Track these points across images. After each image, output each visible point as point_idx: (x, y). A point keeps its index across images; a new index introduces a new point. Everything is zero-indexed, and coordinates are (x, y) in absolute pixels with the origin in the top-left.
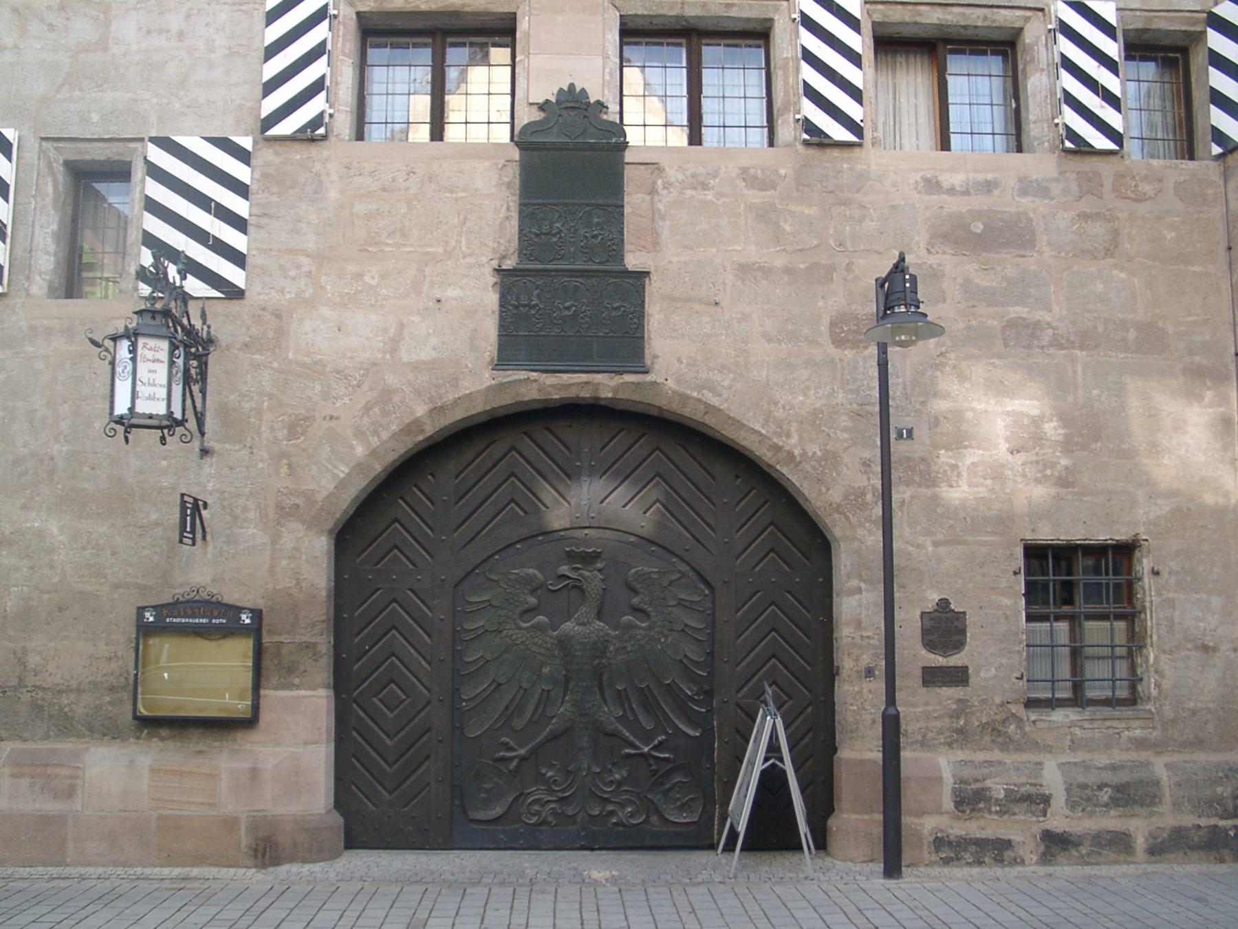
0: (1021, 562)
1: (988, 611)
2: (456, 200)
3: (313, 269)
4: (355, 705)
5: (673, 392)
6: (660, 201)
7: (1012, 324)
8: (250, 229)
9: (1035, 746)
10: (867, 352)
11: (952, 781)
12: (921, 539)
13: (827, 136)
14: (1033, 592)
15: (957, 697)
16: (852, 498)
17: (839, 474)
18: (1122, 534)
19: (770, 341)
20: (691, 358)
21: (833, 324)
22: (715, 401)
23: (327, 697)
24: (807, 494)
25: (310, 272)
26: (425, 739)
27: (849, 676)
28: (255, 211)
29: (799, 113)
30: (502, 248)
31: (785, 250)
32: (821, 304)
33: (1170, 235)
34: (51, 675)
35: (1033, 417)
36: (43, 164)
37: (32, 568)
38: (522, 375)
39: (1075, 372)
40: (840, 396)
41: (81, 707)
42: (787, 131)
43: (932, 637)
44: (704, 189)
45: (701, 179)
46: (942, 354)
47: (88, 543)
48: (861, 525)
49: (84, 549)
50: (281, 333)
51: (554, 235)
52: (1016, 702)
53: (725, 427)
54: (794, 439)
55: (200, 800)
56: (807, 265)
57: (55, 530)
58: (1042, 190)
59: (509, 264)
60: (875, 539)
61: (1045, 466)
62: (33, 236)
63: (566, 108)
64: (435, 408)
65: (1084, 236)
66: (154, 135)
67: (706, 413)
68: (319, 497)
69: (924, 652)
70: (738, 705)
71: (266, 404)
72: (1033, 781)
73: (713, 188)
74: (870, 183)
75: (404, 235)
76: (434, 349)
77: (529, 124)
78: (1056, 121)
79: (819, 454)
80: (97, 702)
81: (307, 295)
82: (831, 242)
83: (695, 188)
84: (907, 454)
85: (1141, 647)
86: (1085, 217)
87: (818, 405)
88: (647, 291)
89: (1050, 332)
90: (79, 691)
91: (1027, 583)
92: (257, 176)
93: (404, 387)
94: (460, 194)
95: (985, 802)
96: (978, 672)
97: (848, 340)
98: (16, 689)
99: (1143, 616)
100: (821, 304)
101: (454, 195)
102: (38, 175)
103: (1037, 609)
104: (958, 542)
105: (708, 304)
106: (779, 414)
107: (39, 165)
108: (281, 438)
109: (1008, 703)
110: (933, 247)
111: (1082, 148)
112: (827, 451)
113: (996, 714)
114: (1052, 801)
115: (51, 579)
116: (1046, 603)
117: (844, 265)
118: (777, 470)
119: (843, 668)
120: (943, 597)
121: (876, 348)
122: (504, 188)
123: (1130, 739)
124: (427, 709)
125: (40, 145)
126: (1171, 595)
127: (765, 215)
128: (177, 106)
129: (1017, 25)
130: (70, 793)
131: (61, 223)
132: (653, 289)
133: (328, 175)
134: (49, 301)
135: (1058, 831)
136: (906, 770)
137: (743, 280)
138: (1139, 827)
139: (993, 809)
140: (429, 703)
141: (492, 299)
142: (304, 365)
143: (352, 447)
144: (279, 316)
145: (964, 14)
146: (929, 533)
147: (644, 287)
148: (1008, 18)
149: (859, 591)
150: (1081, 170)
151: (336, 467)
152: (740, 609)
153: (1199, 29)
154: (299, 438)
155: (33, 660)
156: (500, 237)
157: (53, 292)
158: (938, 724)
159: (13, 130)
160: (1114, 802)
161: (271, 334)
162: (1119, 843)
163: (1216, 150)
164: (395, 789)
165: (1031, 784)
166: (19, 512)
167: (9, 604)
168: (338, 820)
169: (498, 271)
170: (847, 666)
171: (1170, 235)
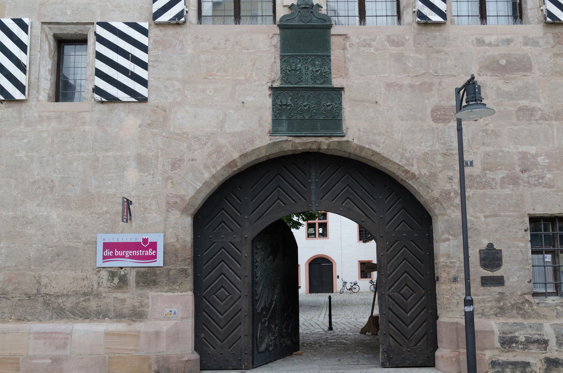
0: (527, 225)
1: (513, 249)
2: (250, 54)
3: (181, 87)
4: (204, 299)
5: (356, 145)
6: (348, 53)
7: (521, 109)
8: (149, 68)
9: (538, 315)
10: (450, 124)
11: (498, 333)
12: (478, 214)
13: (429, 19)
14: (534, 239)
15: (499, 291)
16: (444, 195)
17: (437, 183)
19: (402, 120)
20: (365, 129)
21: (433, 111)
23: (192, 295)
24: (421, 193)
25: (180, 89)
26: (239, 314)
27: (445, 281)
28: (151, 59)
29: (415, 8)
30: (273, 77)
31: (409, 76)
34: (53, 287)
35: (532, 154)
36: (43, 36)
37: (43, 235)
38: (285, 138)
39: (553, 132)
40: (437, 146)
41: (68, 304)
42: (408, 17)
43: (486, 262)
44: (369, 47)
45: (368, 42)
46: (486, 124)
47: (72, 222)
48: (449, 208)
49: (69, 225)
50: (166, 119)
51: (298, 71)
52: (528, 293)
53: (382, 161)
55: (130, 348)
56: (419, 83)
57: (55, 216)
58: (535, 43)
59: (276, 85)
60: (458, 214)
61: (539, 178)
62: (39, 71)
63: (302, 8)
64: (243, 155)
65: (556, 65)
66: (99, 21)
67: (372, 155)
68: (187, 198)
69: (481, 269)
71: (160, 153)
72: (539, 333)
74: (450, 42)
75: (225, 71)
76: (242, 126)
77: (284, 16)
78: (542, 8)
79: (427, 174)
80: (77, 301)
81: (179, 100)
83: (365, 47)
84: (471, 173)
87: (426, 151)
88: (343, 96)
89: (540, 112)
90: (68, 295)
91: (531, 235)
92: (151, 41)
93: (227, 145)
94: (252, 51)
95: (516, 344)
96: (509, 279)
97: (440, 119)
98: (35, 295)
101: (249, 51)
102: (41, 41)
104: (496, 216)
105: (373, 103)
106: (408, 155)
107: (41, 36)
108: (168, 170)
109: (524, 294)
110: (481, 72)
112: (431, 172)
113: (518, 299)
114: (549, 343)
115: (53, 240)
117: (438, 82)
118: (406, 182)
119: (441, 277)
120: (490, 242)
121: (456, 122)
122: (273, 47)
124: (239, 300)
125: (42, 26)
127: (399, 58)
128: (110, 7)
130: (64, 346)
131: (53, 64)
132: (346, 96)
133: (187, 41)
134: (49, 103)
135: (553, 358)
136: (477, 327)
137: (389, 91)
139: (520, 347)
140: (240, 297)
141: (269, 102)
142: (178, 134)
143: (203, 174)
144: (165, 111)
146: (482, 211)
147: (341, 96)
149: (448, 240)
150: (554, 32)
151: (195, 184)
152: (389, 249)
154: (176, 170)
155: (44, 281)
156: (272, 72)
157: (49, 99)
158: (489, 304)
159: (28, 19)
161: (161, 119)
164: (224, 340)
165: (538, 334)
166: (36, 208)
167: (32, 253)
168: (196, 356)
169: (271, 88)
170: (443, 276)
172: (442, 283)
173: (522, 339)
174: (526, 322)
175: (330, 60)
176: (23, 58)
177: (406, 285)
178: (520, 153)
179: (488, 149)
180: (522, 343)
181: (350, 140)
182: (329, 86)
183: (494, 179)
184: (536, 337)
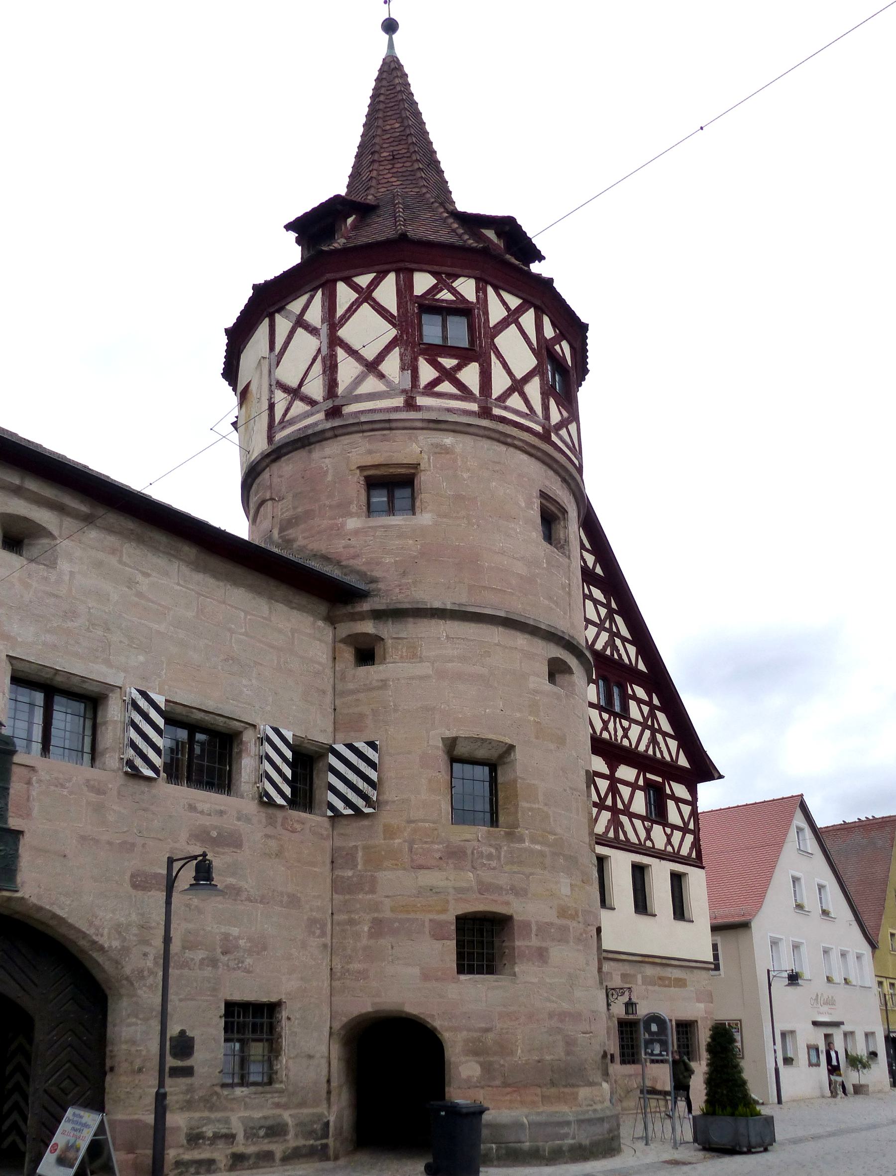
14: (228, 1028)
17: (130, 959)
18: (274, 999)
21: (132, 876)
45: (61, 781)
54: (105, 938)
58: (248, 820)
70: (45, 1091)
73: (67, 788)
78: (258, 785)
83: (56, 786)
85: (277, 1057)
86: (267, 836)
89: (246, 893)
99: (280, 1040)
103: (230, 1036)
104: (192, 1000)
116: (232, 1032)
123: (273, 1103)
126: (295, 1030)
127: (99, 809)
129: (240, 730)
138: (278, 1149)
149: (137, 1024)
160: (267, 1135)
162: (266, 1157)
163: (330, 813)
172: (121, 1074)
173: (210, 1134)
174: (213, 1116)
175: (8, 794)
176: (133, 734)
177: (69, 1077)
178: (222, 934)
179: (191, 926)
180: (209, 1139)
181: (27, 896)
182: (4, 826)
183: (193, 959)
184: (224, 1131)
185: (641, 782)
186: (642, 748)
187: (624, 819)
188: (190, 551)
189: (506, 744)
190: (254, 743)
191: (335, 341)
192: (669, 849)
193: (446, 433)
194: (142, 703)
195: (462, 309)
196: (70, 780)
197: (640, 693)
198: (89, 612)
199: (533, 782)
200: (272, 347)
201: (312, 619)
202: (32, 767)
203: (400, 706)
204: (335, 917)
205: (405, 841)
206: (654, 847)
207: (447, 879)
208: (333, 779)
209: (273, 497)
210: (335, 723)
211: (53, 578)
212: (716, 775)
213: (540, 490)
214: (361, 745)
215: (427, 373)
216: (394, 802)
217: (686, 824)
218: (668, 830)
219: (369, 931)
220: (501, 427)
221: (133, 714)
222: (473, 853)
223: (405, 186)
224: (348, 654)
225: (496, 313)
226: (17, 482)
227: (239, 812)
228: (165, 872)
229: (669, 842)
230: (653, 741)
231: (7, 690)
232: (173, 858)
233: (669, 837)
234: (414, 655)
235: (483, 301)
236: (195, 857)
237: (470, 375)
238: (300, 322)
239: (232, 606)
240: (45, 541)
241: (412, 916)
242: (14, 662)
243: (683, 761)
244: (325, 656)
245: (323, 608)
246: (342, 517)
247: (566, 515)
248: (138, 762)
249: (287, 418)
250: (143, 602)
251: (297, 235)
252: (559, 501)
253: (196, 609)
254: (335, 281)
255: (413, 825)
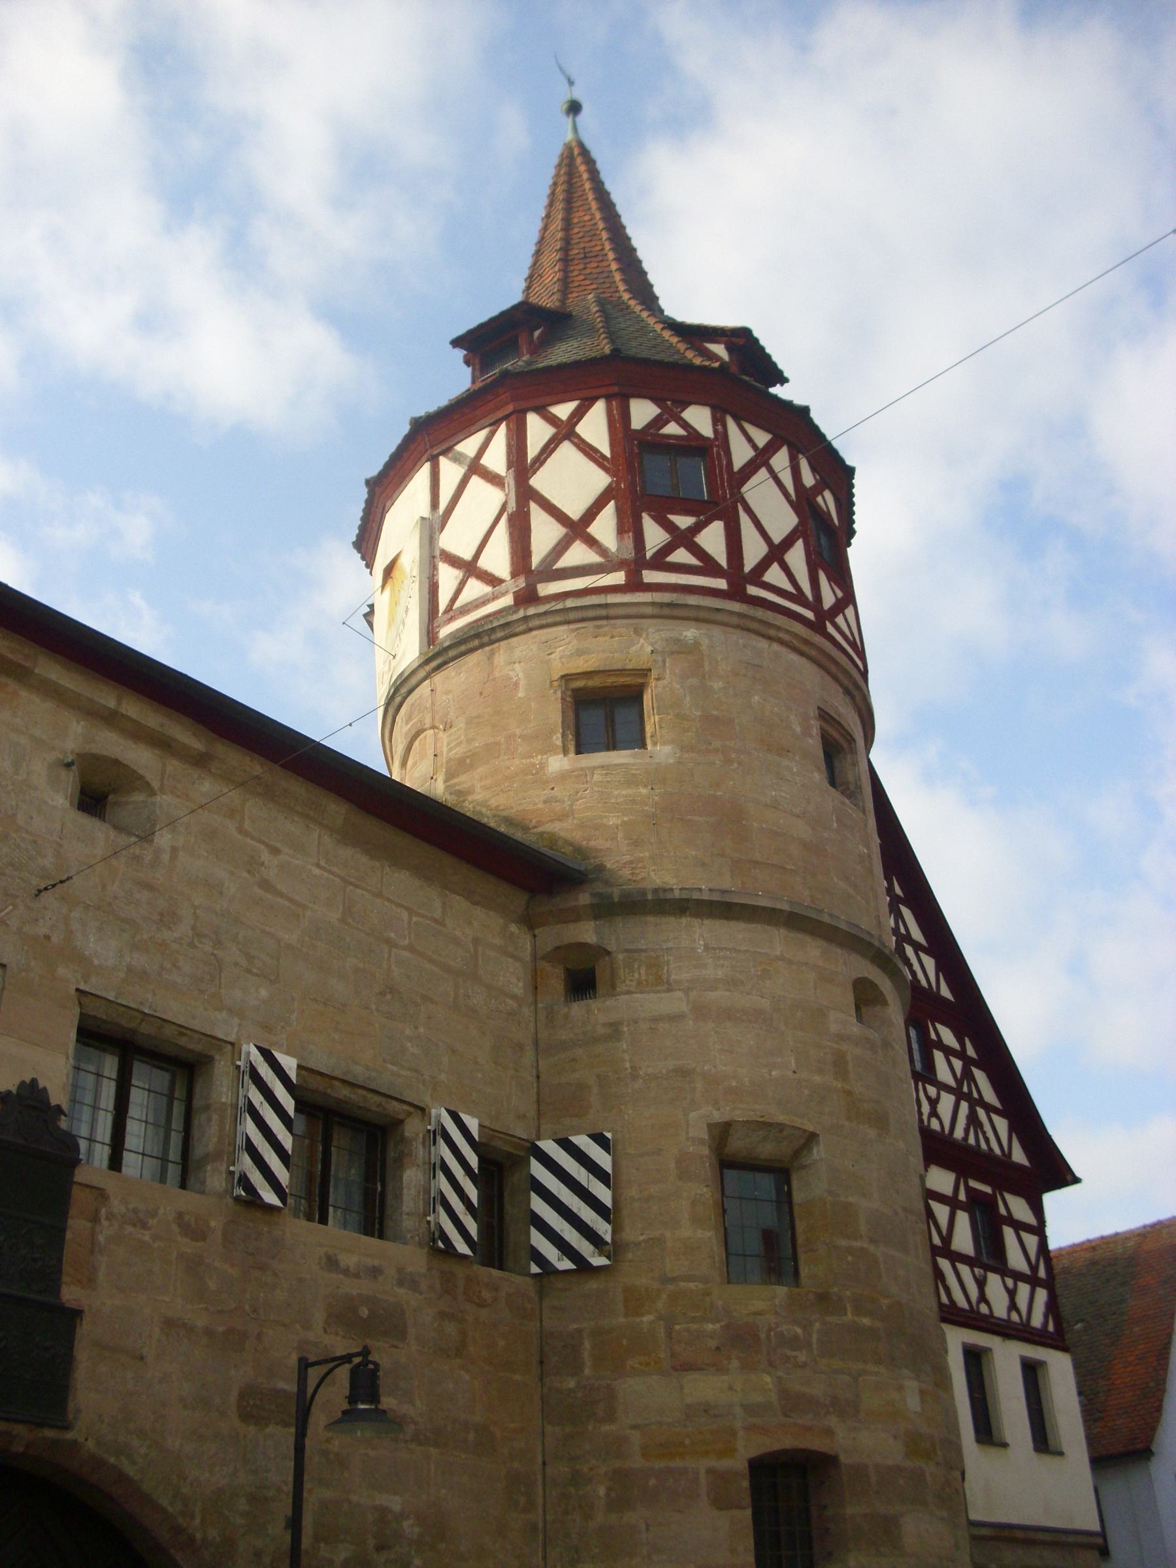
21: (242, 1396)
22: (130, 1471)
32: (233, 1372)
33: (502, 1343)
45: (141, 1215)
73: (149, 1229)
82: (247, 1307)
83: (135, 1225)
100: (233, 1372)
111: (253, 1200)
129: (401, 1117)
132: (86, 1330)
145: (364, 1097)
148: (396, 1109)
153: (522, 1153)
163: (535, 1269)
171: (502, 1343)
185: (962, 1196)
186: (959, 1133)
187: (944, 1264)
188: (337, 809)
189: (805, 1131)
190: (421, 1140)
191: (526, 495)
192: (1015, 1317)
193: (679, 622)
194: (265, 1071)
195: (693, 445)
196: (154, 1214)
197: (948, 1036)
198: (195, 913)
199: (851, 1199)
200: (435, 504)
201: (501, 921)
202: (99, 1189)
203: (640, 1068)
204: (549, 1470)
205: (660, 1318)
206: (991, 1314)
207: (731, 1388)
208: (538, 1205)
209: (437, 724)
210: (538, 1102)
211: (148, 858)
212: (1069, 1178)
213: (819, 708)
214: (582, 1141)
215: (654, 536)
216: (639, 1243)
217: (1034, 1268)
218: (1010, 1282)
219: (608, 1495)
220: (760, 613)
221: (251, 1091)
222: (768, 1337)
223: (584, 288)
224: (556, 982)
225: (741, 453)
226: (112, 704)
227: (400, 1270)
228: (292, 1388)
229: (1013, 1306)
230: (973, 1120)
231: (71, 1051)
232: (307, 1359)
233: (1012, 1293)
234: (659, 980)
235: (722, 437)
236: (347, 1358)
237: (713, 539)
238: (475, 468)
239: (392, 902)
240: (138, 797)
241: (678, 1463)
242: (85, 1000)
243: (1019, 1156)
244: (521, 984)
245: (518, 900)
246: (542, 754)
247: (853, 745)
248: (256, 1178)
249: (457, 604)
250: (269, 896)
251: (465, 352)
252: (843, 722)
253: (341, 907)
254: (524, 412)
255: (671, 1287)
